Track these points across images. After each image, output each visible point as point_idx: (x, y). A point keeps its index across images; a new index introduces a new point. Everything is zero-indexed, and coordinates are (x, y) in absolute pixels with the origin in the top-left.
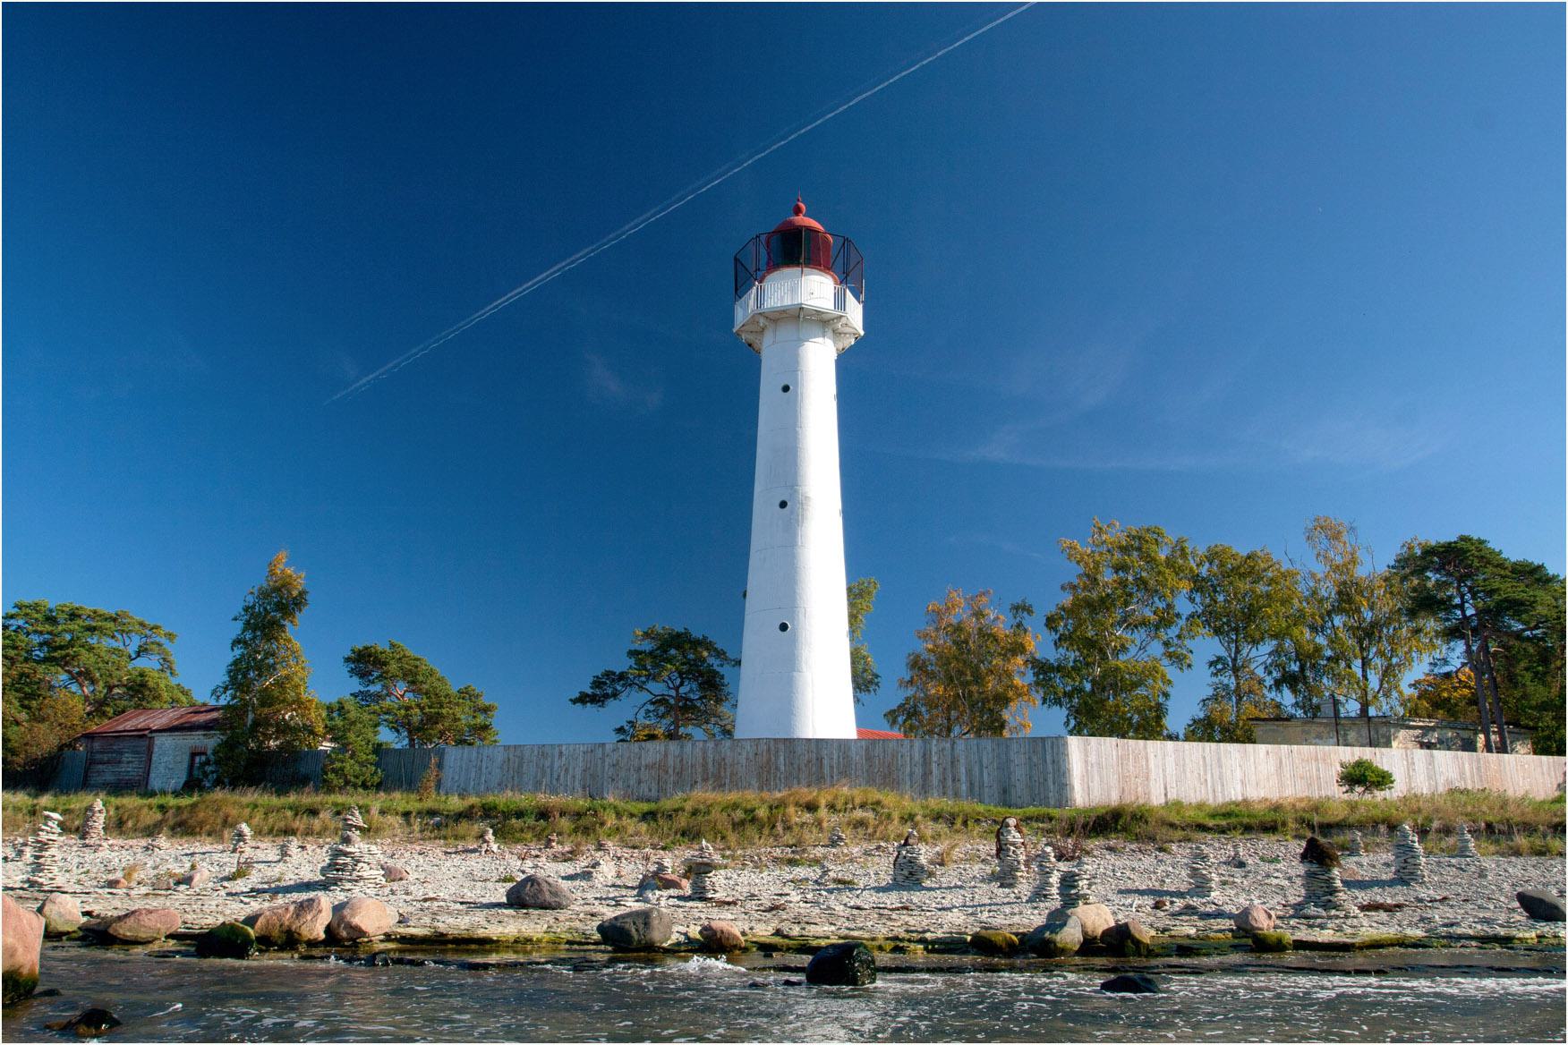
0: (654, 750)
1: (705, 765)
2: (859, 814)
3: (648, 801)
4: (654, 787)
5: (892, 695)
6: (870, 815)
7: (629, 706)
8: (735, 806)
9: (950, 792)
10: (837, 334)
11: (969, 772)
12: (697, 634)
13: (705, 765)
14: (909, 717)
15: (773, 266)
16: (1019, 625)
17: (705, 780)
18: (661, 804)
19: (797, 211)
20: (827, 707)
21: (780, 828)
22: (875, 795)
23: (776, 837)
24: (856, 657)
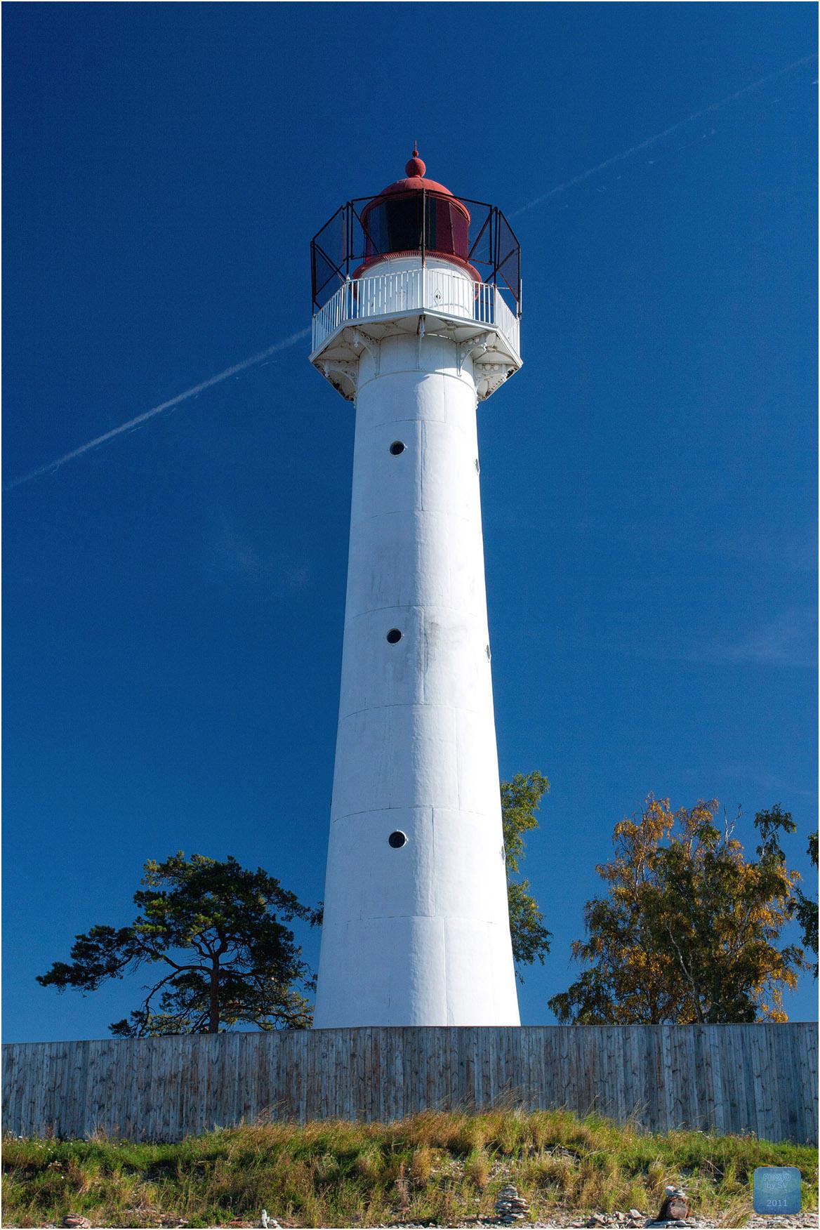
0: (172, 1055)
1: (263, 1078)
2: (546, 1160)
3: (161, 1142)
4: (174, 1118)
5: (565, 970)
6: (567, 1161)
7: (136, 986)
8: (320, 1148)
9: (697, 1120)
10: (479, 365)
11: (728, 1084)
12: (249, 866)
13: (263, 1078)
14: (589, 1005)
15: (373, 256)
16: (771, 847)
17: (263, 1104)
18: (185, 1145)
19: (413, 170)
20: (474, 977)
21: (402, 1188)
22: (572, 1126)
23: (396, 1205)
24: (512, 890)
